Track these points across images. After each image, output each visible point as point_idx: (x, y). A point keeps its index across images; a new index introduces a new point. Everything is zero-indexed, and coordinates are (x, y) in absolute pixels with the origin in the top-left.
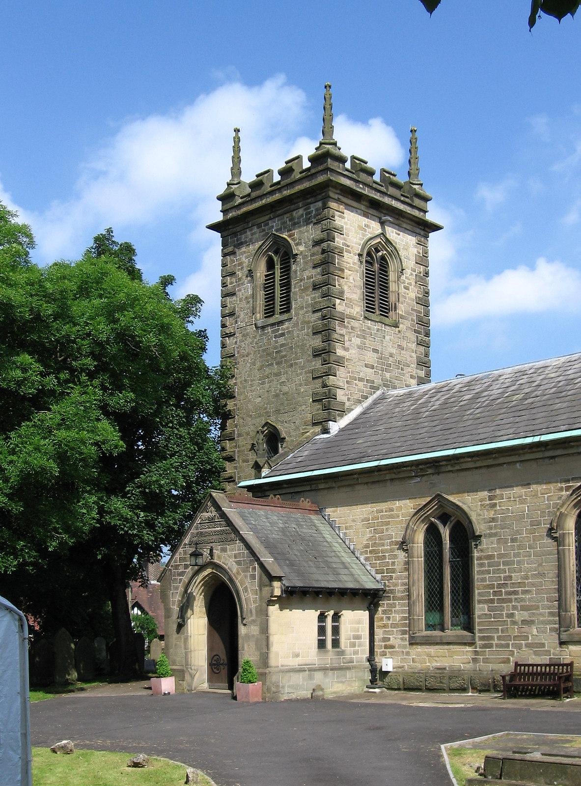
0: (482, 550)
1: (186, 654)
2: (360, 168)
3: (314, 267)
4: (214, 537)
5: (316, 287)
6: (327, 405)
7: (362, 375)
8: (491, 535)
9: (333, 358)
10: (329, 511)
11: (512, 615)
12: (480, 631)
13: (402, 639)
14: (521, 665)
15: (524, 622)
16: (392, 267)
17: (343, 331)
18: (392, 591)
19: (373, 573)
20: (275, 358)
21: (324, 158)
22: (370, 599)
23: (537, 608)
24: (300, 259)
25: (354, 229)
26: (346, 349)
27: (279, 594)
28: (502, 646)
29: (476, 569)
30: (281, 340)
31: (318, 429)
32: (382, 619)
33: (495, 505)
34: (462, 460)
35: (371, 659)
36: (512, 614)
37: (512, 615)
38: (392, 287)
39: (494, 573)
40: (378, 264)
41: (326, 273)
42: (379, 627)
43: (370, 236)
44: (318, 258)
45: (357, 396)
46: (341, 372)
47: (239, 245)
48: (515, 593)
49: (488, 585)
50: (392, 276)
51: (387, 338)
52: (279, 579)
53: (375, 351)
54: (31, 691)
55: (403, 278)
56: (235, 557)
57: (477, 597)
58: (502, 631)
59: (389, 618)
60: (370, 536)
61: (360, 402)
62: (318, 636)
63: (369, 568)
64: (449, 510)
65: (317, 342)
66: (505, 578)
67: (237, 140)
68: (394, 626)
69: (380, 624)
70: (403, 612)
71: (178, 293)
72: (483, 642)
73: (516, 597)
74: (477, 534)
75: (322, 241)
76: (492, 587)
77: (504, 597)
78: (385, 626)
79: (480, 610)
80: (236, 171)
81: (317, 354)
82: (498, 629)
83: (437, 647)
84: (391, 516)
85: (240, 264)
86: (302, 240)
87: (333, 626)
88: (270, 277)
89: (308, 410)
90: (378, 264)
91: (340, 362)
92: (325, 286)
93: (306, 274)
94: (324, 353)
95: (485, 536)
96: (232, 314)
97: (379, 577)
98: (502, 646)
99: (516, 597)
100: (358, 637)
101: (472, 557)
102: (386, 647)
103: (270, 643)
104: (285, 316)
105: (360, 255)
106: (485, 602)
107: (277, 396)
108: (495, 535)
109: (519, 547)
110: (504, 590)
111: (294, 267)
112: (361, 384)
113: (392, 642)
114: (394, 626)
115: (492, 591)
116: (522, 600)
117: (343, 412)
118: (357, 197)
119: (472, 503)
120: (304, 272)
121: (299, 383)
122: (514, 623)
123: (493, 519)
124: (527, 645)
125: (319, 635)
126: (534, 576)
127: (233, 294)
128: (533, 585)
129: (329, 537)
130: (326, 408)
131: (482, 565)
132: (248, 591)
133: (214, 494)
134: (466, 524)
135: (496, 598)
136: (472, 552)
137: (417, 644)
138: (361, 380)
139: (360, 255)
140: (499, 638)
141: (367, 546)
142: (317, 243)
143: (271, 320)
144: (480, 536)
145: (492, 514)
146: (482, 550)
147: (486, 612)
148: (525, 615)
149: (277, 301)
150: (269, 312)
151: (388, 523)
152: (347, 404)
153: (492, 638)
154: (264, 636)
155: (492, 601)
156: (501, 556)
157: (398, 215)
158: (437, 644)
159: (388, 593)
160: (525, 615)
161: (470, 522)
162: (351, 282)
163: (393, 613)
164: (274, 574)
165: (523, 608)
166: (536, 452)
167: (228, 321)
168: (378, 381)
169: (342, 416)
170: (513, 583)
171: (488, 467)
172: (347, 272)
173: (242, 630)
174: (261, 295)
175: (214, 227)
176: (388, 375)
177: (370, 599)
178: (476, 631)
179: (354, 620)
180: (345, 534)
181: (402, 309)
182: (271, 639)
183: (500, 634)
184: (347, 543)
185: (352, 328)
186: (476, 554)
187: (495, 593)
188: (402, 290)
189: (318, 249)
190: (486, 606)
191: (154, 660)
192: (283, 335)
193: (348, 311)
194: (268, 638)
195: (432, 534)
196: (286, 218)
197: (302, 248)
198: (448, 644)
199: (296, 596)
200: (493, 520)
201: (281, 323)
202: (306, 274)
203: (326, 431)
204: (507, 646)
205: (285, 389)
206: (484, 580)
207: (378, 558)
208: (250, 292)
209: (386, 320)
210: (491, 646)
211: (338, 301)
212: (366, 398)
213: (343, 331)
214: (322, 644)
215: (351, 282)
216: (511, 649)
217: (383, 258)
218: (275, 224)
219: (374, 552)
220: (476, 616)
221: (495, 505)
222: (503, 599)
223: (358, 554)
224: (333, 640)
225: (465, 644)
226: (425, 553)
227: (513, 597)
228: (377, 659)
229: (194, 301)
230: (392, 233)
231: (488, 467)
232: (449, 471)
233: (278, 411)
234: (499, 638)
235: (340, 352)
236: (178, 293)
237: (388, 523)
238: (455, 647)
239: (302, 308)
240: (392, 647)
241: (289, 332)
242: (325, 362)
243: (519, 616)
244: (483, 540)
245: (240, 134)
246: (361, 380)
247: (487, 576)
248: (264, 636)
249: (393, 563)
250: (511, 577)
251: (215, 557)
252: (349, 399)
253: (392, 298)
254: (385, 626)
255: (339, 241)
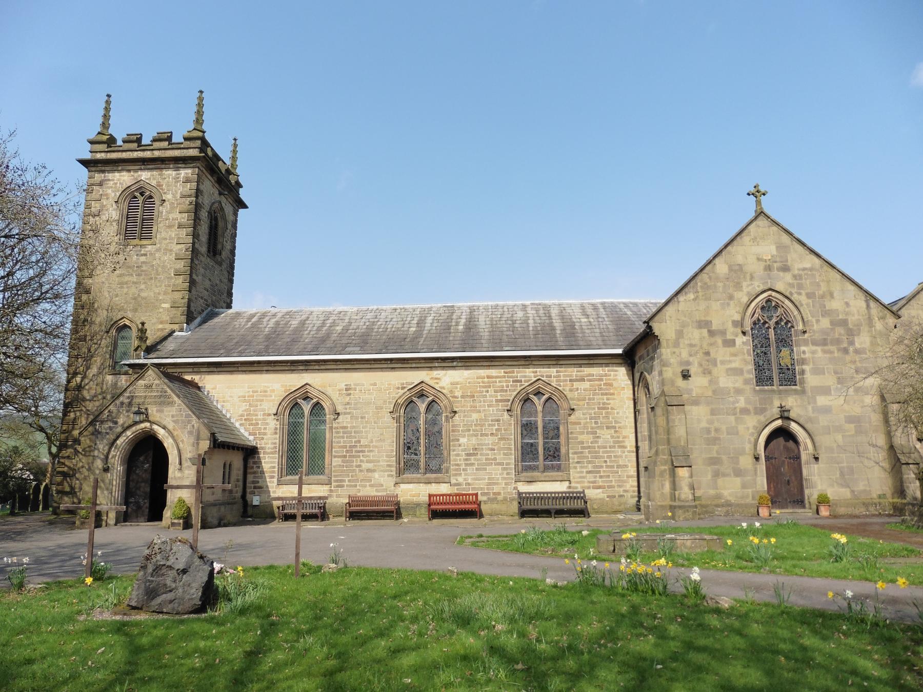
8: (345, 413)
11: (360, 466)
14: (434, 495)
15: (369, 470)
23: (379, 461)
28: (351, 486)
30: (143, 259)
33: (350, 394)
35: (244, 496)
37: (360, 466)
48: (362, 451)
53: (210, 280)
54: (161, 520)
56: (173, 416)
61: (200, 313)
76: (346, 447)
80: (105, 125)
84: (266, 396)
98: (351, 486)
106: (339, 457)
108: (349, 413)
109: (367, 422)
116: (368, 456)
122: (361, 471)
124: (370, 486)
126: (377, 441)
128: (376, 447)
131: (338, 433)
141: (242, 415)
145: (347, 399)
148: (370, 466)
151: (262, 401)
153: (344, 481)
155: (345, 456)
156: (353, 427)
165: (368, 462)
192: (145, 255)
200: (348, 403)
204: (356, 486)
205: (143, 294)
207: (252, 424)
210: (343, 486)
228: (248, 496)
234: (349, 481)
237: (262, 401)
241: (151, 254)
243: (365, 466)
245: (111, 99)
249: (265, 429)
253: (219, 247)
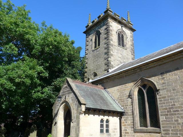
0: (160, 95)
1: (57, 133)
3: (105, 34)
4: (67, 92)
5: (105, 39)
7: (118, 59)
8: (163, 89)
9: (110, 54)
10: (108, 90)
11: (177, 120)
12: (163, 127)
13: (131, 130)
16: (125, 37)
17: (113, 48)
18: (127, 113)
19: (121, 107)
20: (97, 57)
22: (120, 114)
24: (102, 34)
26: (114, 53)
27: (84, 111)
29: (158, 102)
30: (98, 53)
31: (106, 71)
32: (124, 122)
33: (164, 78)
34: (149, 65)
36: (177, 120)
37: (177, 120)
38: (125, 41)
39: (167, 103)
42: (123, 125)
43: (119, 29)
44: (106, 32)
45: (117, 64)
46: (112, 57)
47: (89, 35)
49: (165, 108)
50: (125, 39)
51: (124, 52)
52: (85, 104)
55: (127, 39)
57: (160, 113)
58: (173, 127)
59: (126, 122)
62: (101, 128)
63: (119, 105)
64: (146, 83)
65: (106, 51)
66: (172, 105)
68: (129, 125)
69: (124, 124)
70: (131, 120)
71: (76, 46)
72: (165, 132)
73: (178, 112)
74: (158, 89)
76: (166, 109)
77: (172, 113)
78: (125, 125)
79: (162, 118)
82: (171, 126)
83: (145, 134)
85: (90, 39)
86: (102, 30)
87: (106, 125)
88: (96, 40)
89: (104, 67)
91: (112, 55)
93: (104, 36)
94: (107, 53)
95: (161, 90)
96: (87, 50)
97: (122, 108)
99: (178, 112)
100: (116, 129)
101: (156, 98)
102: (126, 133)
103: (80, 130)
104: (99, 47)
105: (116, 32)
107: (97, 65)
108: (166, 89)
110: (172, 110)
111: (101, 36)
112: (117, 61)
113: (128, 131)
114: (129, 125)
115: (166, 111)
117: (113, 67)
119: (154, 80)
120: (103, 36)
121: (102, 62)
123: (164, 83)
125: (101, 127)
127: (88, 45)
129: (106, 96)
130: (108, 66)
131: (161, 101)
133: (68, 79)
134: (153, 87)
135: (169, 113)
136: (156, 96)
137: (137, 132)
138: (118, 60)
139: (116, 32)
140: (172, 130)
141: (118, 98)
143: (96, 49)
144: (159, 90)
145: (163, 81)
146: (160, 95)
147: (165, 119)
151: (125, 90)
152: (114, 66)
154: (78, 127)
155: (167, 115)
156: (169, 96)
158: (145, 132)
159: (126, 113)
161: (155, 85)
162: (114, 38)
163: (127, 120)
164: (82, 103)
166: (180, 55)
167: (86, 51)
168: (122, 61)
169: (113, 68)
170: (176, 107)
171: (160, 65)
172: (113, 35)
173: (72, 124)
176: (124, 60)
177: (120, 114)
178: (161, 127)
179: (114, 121)
180: (112, 95)
181: (127, 46)
182: (80, 128)
183: (172, 129)
184: (112, 98)
185: (115, 48)
186: (158, 97)
187: (168, 112)
188: (127, 42)
189: (106, 30)
190: (165, 117)
193: (114, 44)
194: (79, 128)
195: (140, 92)
196: (99, 26)
197: (102, 31)
198: (150, 132)
199: (89, 111)
201: (98, 48)
202: (104, 36)
203: (108, 72)
206: (162, 106)
207: (122, 102)
209: (124, 48)
210: (169, 134)
211: (111, 41)
212: (119, 65)
213: (113, 48)
214: (102, 131)
215: (114, 38)
216: (178, 135)
217: (122, 35)
218: (97, 28)
219: (121, 100)
220: (160, 121)
221: (164, 78)
222: (172, 114)
223: (116, 101)
224: (106, 130)
225: (157, 133)
226: (138, 99)
227: (176, 113)
229: (80, 49)
230: (124, 29)
231: (160, 65)
232: (145, 69)
233: (97, 69)
234: (172, 130)
235: (112, 53)
236: (76, 46)
237: (125, 90)
238: (152, 134)
239: (102, 44)
240: (128, 133)
244: (160, 91)
246: (118, 60)
247: (164, 105)
248: (78, 127)
250: (174, 105)
251: (66, 99)
252: (114, 64)
253: (125, 44)
254: (125, 125)
255: (111, 28)
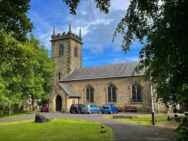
2: (74, 35)
6: (69, 69)
16: (78, 49)
21: (69, 33)
24: (65, 48)
25: (73, 44)
30: (62, 59)
40: (76, 49)
41: (69, 50)
60: (79, 89)
67: (80, 31)
75: (69, 46)
81: (68, 62)
89: (66, 70)
90: (76, 49)
92: (69, 52)
94: (69, 62)
117: (71, 71)
118: (74, 39)
120: (66, 50)
132: (63, 97)
142: (68, 46)
148: (101, 100)
149: (61, 53)
150: (60, 54)
157: (79, 42)
160: (101, 100)
173: (63, 103)
174: (58, 52)
175: (50, 41)
191: (38, 41)
208: (57, 52)
230: (78, 44)
242: (69, 63)
255: (71, 46)
